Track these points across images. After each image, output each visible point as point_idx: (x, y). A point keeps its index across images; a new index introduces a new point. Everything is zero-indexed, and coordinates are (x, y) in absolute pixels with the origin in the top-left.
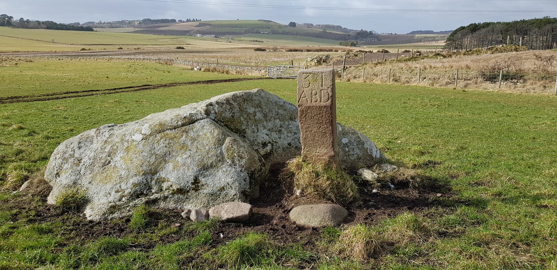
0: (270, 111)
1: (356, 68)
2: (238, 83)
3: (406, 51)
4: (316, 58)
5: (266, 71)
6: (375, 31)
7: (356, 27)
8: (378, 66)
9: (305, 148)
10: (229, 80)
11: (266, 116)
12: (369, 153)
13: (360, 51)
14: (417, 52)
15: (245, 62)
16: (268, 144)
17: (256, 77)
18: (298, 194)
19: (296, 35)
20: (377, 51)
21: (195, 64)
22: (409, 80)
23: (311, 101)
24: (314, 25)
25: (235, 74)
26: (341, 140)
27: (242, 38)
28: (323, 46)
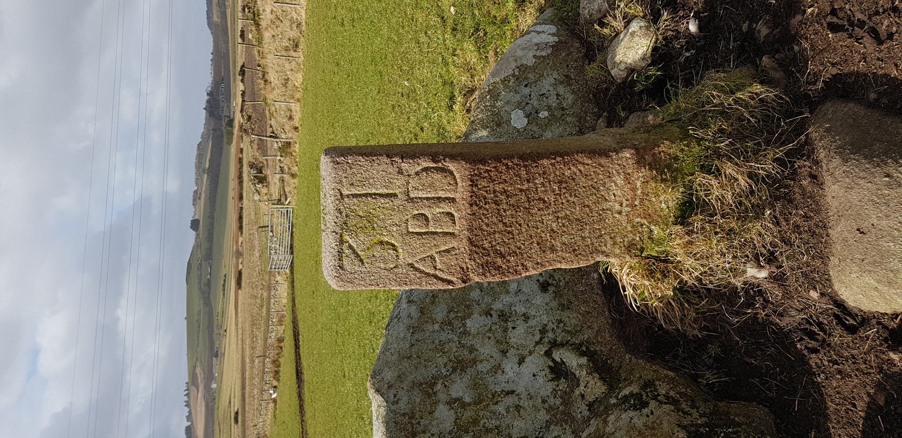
0: (440, 348)
1: (273, 116)
2: (301, 325)
3: (242, 36)
4: (255, 186)
5: (279, 273)
6: (206, 87)
7: (201, 117)
8: (269, 79)
9: (603, 252)
10: (295, 340)
11: (459, 362)
12: (549, 52)
13: (242, 111)
14: (244, 11)
15: (262, 306)
16: (553, 360)
17: (290, 292)
18: (763, 274)
19: (213, 218)
20: (241, 84)
21: (265, 397)
22: (296, 24)
23: (448, 238)
24: (196, 188)
25: (283, 327)
26: (518, 131)
27: (220, 310)
28: (233, 173)
